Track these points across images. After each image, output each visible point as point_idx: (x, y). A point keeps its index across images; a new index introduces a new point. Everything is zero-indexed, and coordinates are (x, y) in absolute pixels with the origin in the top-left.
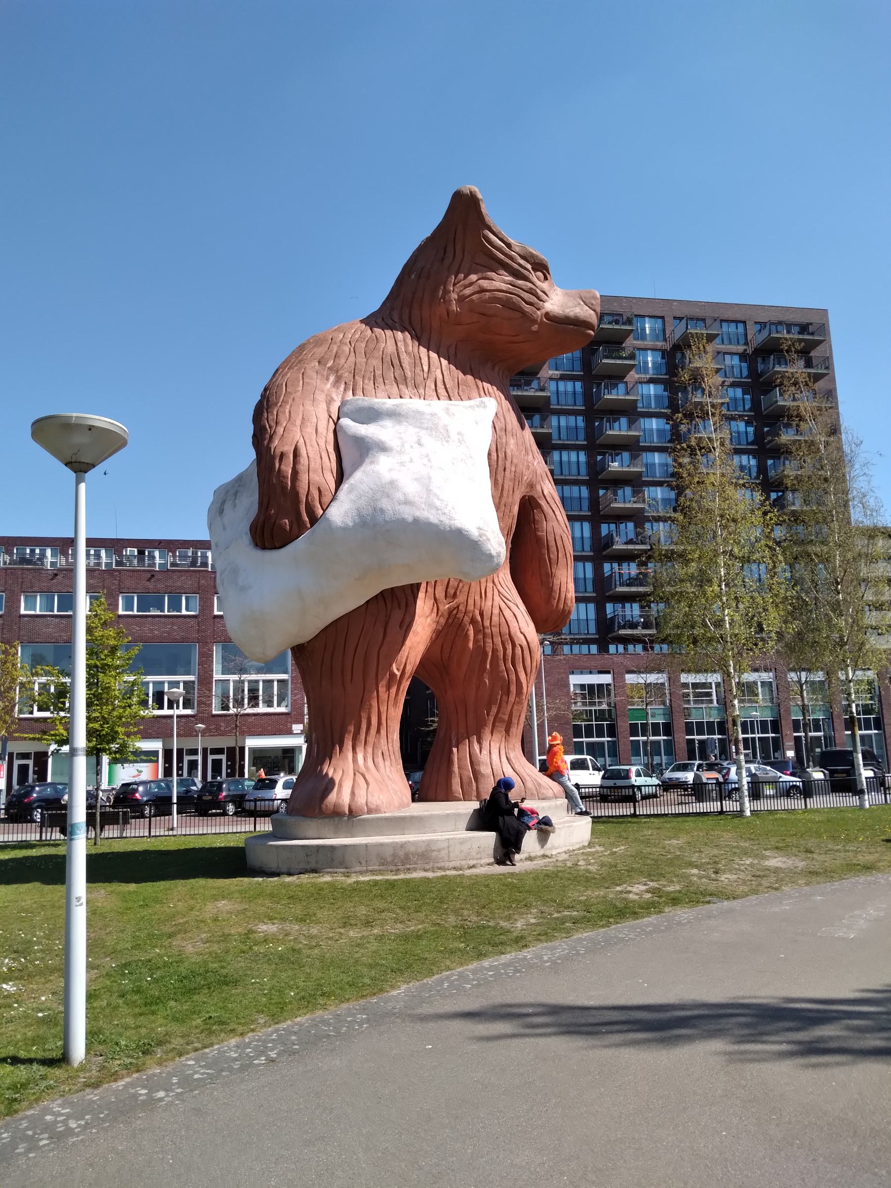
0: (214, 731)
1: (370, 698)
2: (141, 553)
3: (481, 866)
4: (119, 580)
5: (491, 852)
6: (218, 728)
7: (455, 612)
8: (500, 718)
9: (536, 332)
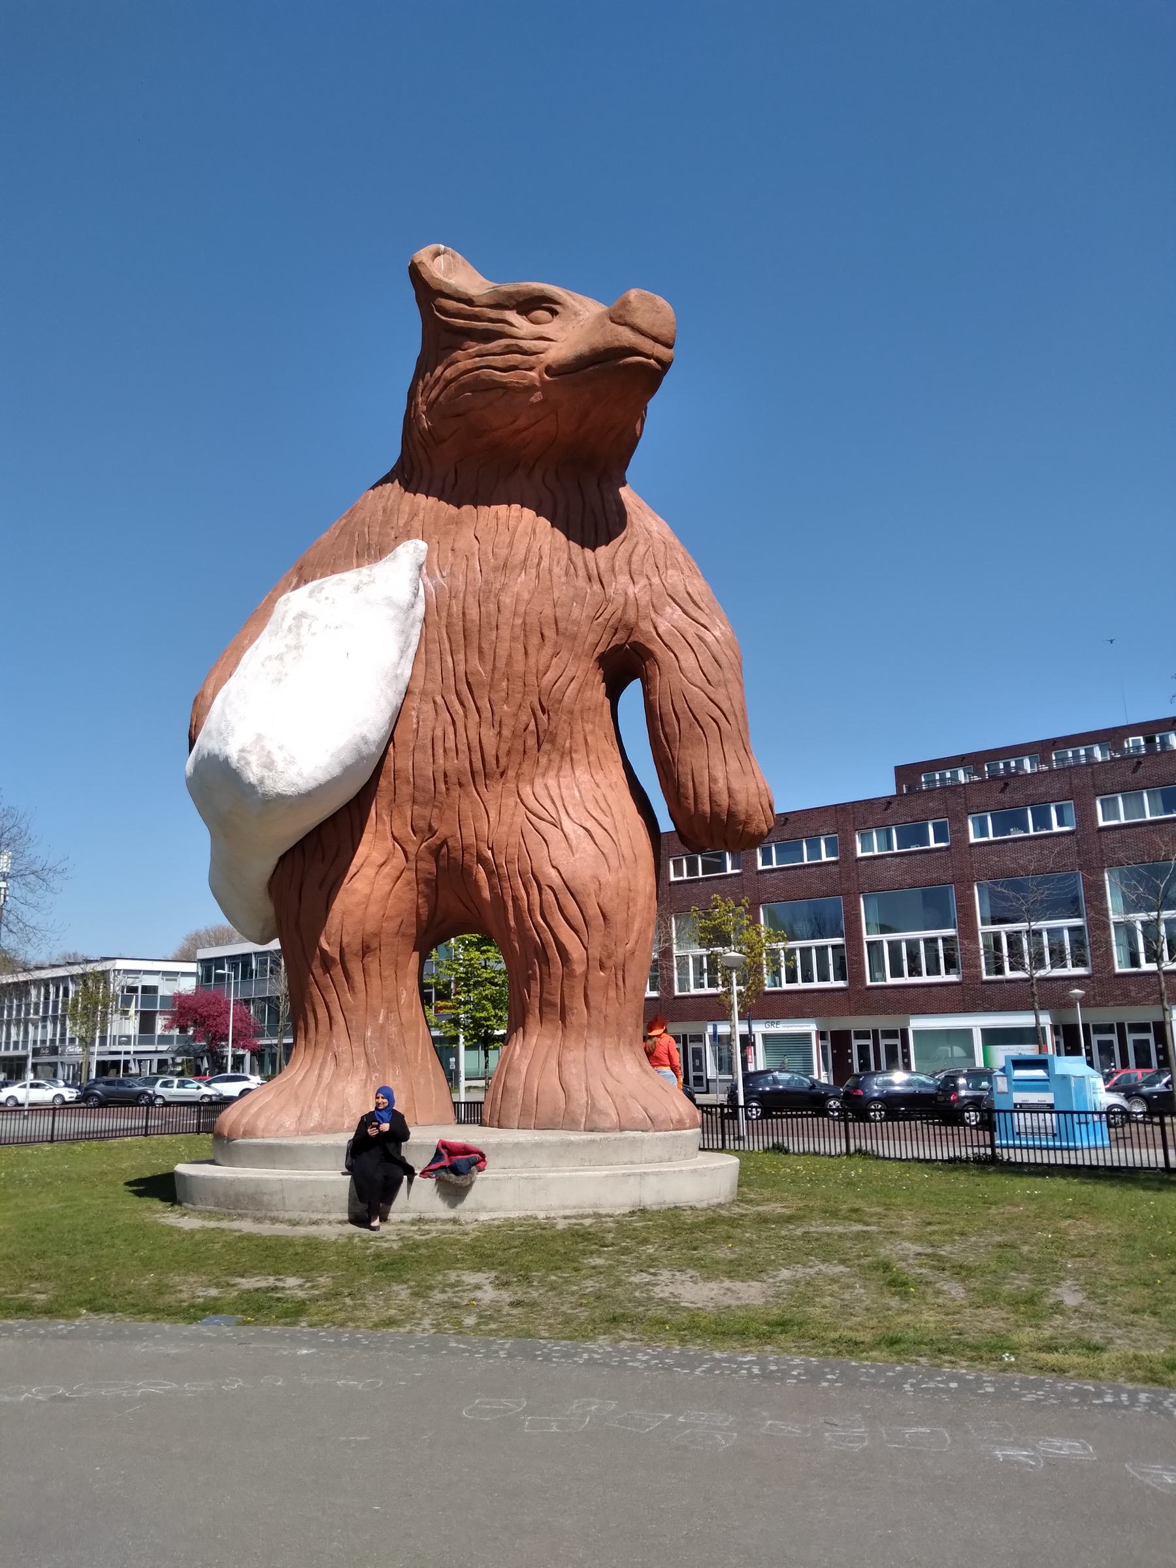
0: (1120, 998)
1: (308, 985)
2: (1150, 741)
3: (330, 1223)
4: (965, 797)
5: (345, 1203)
6: (1126, 994)
7: (444, 850)
8: (546, 999)
9: (542, 402)
